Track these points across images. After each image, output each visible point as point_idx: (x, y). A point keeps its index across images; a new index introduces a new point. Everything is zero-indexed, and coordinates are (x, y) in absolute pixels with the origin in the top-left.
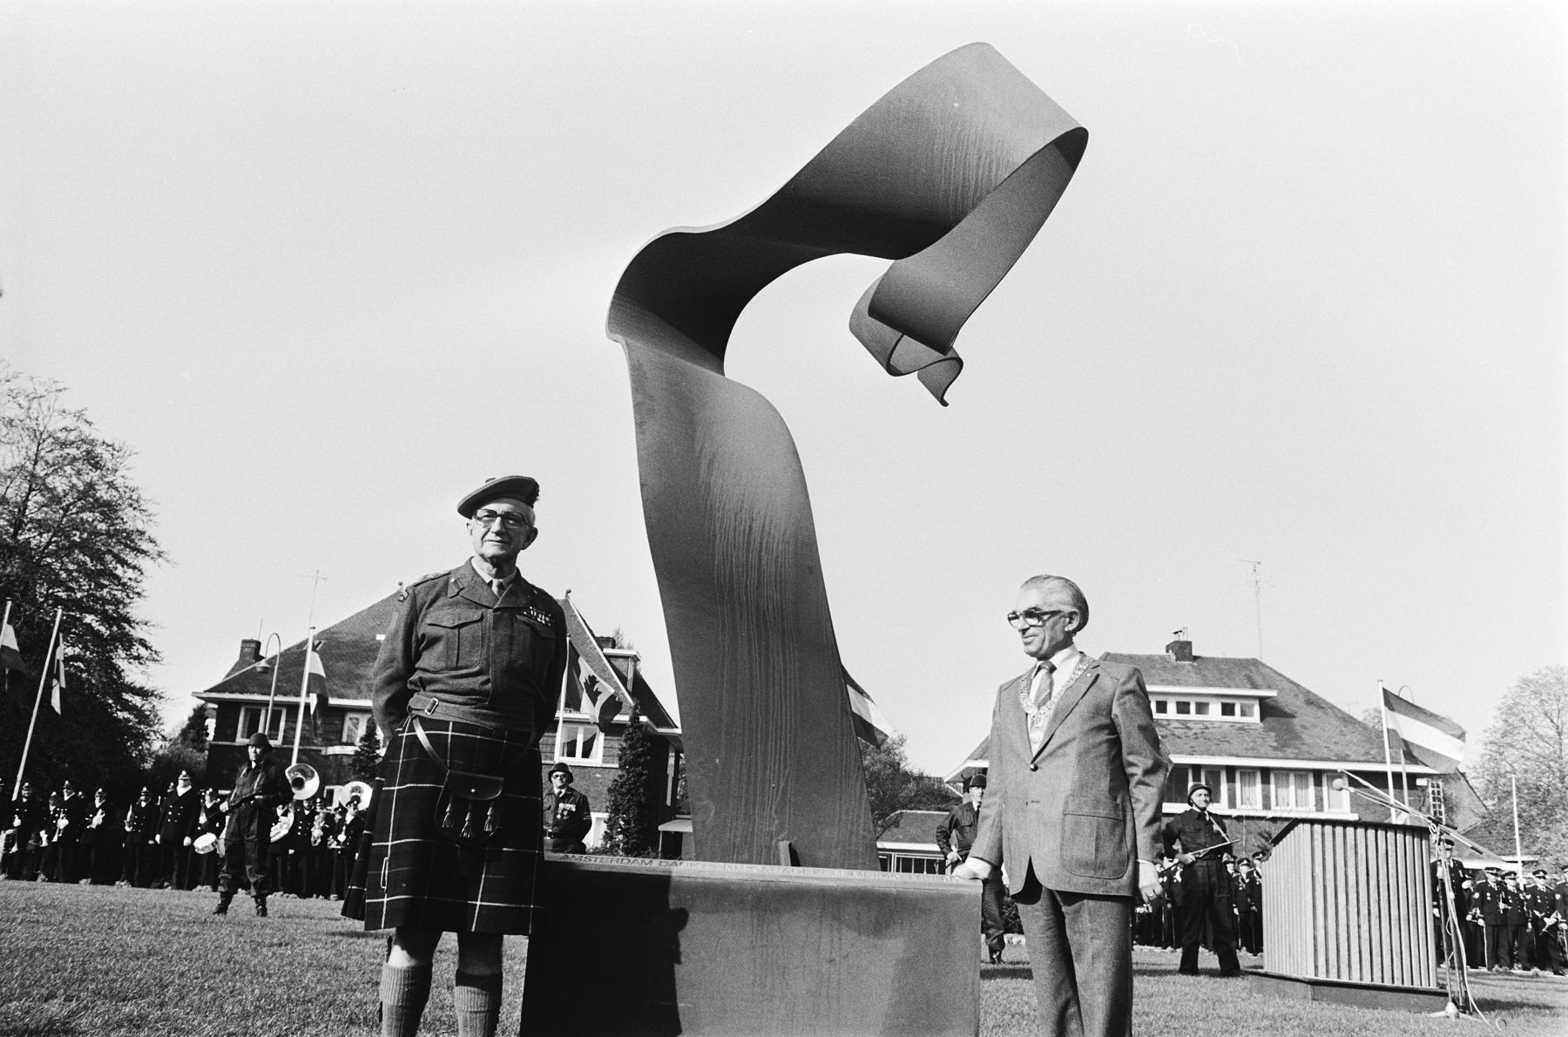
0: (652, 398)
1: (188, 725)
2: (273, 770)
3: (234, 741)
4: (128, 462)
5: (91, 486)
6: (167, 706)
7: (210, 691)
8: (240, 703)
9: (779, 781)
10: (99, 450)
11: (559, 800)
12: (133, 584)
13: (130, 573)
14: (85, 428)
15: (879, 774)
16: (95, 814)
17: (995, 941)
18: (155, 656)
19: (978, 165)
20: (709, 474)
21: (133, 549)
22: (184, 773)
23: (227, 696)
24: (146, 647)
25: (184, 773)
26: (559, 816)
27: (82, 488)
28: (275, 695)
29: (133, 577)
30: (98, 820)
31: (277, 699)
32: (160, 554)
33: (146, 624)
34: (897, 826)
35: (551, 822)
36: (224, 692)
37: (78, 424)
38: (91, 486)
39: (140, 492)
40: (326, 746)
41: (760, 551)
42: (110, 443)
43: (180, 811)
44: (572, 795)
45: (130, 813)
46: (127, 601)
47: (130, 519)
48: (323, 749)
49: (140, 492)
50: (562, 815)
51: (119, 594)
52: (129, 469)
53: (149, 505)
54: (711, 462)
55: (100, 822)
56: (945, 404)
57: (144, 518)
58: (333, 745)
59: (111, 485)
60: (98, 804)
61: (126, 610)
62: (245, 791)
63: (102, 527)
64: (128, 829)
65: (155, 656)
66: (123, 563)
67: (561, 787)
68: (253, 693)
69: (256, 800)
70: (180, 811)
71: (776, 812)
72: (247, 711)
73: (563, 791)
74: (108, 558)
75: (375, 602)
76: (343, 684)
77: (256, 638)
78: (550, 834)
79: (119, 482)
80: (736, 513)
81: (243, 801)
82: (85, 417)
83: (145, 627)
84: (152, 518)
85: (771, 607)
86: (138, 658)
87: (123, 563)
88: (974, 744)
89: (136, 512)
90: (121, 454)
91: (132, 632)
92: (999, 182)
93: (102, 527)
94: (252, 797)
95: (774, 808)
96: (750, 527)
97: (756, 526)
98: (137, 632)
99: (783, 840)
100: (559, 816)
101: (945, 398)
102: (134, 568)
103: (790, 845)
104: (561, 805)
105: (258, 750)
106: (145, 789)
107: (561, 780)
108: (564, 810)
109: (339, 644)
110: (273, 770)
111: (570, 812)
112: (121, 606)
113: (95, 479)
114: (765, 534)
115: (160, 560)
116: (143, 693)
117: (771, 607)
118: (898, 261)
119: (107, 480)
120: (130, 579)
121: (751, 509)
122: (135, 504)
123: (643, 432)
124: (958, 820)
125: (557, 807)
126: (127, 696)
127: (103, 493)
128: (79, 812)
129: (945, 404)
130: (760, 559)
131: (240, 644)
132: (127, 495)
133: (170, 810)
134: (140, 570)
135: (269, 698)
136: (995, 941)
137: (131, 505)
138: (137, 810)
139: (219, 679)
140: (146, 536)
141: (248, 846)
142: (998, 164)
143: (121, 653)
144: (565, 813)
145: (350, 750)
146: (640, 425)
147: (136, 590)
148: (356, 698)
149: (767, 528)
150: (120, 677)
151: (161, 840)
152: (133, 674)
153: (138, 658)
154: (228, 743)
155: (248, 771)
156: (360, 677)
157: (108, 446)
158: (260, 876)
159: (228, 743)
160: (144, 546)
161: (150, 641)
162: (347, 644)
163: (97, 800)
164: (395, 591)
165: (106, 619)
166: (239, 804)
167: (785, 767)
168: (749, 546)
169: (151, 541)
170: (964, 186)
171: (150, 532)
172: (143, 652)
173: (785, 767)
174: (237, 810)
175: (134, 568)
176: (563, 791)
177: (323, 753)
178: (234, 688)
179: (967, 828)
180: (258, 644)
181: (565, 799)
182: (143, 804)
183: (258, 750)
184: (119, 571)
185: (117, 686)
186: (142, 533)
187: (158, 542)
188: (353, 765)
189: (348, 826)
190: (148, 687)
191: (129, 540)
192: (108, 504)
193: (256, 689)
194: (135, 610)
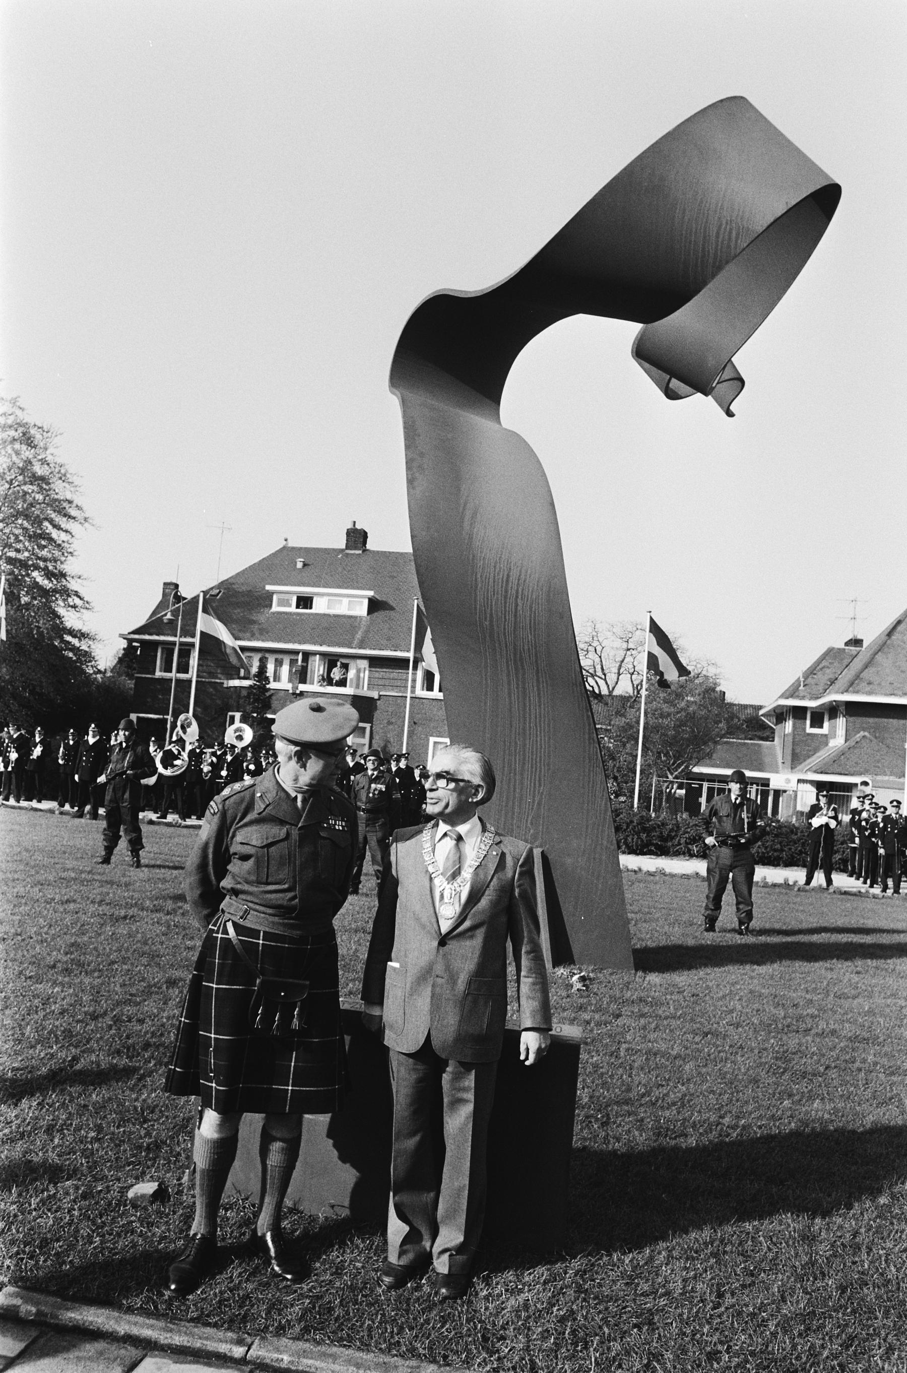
0: (422, 455)
1: (123, 655)
2: (139, 749)
3: (154, 674)
4: (56, 441)
5: (29, 462)
6: (100, 646)
7: (134, 632)
8: (156, 644)
9: (534, 797)
10: (33, 431)
11: (372, 780)
12: (66, 545)
13: (63, 536)
14: (19, 412)
15: (694, 713)
16: (35, 747)
17: (743, 915)
18: (87, 606)
19: (717, 236)
20: (471, 525)
21: (65, 515)
22: (93, 726)
23: (147, 637)
24: (81, 598)
25: (93, 726)
26: (371, 795)
27: (21, 465)
28: (181, 636)
29: (65, 539)
30: (37, 751)
31: (183, 640)
32: (86, 519)
33: (79, 578)
34: (710, 758)
35: (364, 799)
36: (144, 634)
37: (13, 410)
38: (29, 462)
39: (67, 467)
40: (228, 679)
41: (517, 597)
42: (40, 425)
43: (92, 757)
44: (383, 777)
45: (62, 749)
46: (63, 559)
47: (61, 490)
48: (225, 682)
49: (67, 467)
50: (374, 794)
51: (57, 553)
52: (57, 447)
53: (75, 477)
54: (475, 514)
55: (39, 754)
56: (730, 414)
57: (72, 489)
58: (233, 679)
59: (44, 462)
60: (38, 740)
61: (62, 566)
62: (119, 766)
63: (40, 497)
64: (61, 762)
65: (87, 606)
66: (57, 527)
67: (373, 770)
68: (168, 635)
69: (127, 775)
70: (92, 757)
71: (532, 824)
72: (163, 649)
73: (376, 773)
74: (46, 524)
75: (264, 556)
76: (240, 628)
77: (174, 581)
78: (363, 810)
79: (49, 458)
80: (496, 563)
81: (117, 775)
82: (18, 404)
83: (79, 580)
84: (78, 489)
85: (526, 647)
86: (74, 607)
87: (57, 527)
88: (786, 683)
89: (64, 484)
90: (49, 434)
91: (69, 586)
92: (738, 251)
93: (40, 497)
94: (124, 773)
95: (530, 818)
96: (508, 576)
97: (514, 574)
98: (73, 585)
99: (537, 847)
100: (371, 795)
101: (731, 408)
102: (66, 531)
103: (542, 853)
104: (373, 786)
105: (127, 733)
106: (72, 731)
107: (373, 763)
108: (375, 789)
109: (236, 593)
110: (139, 749)
111: (380, 791)
112: (59, 562)
113: (31, 456)
114: (521, 581)
115: (86, 525)
116: (81, 635)
117: (526, 647)
118: (650, 325)
119: (40, 457)
120: (63, 541)
121: (509, 563)
122: (63, 478)
123: (414, 488)
124: (716, 810)
125: (370, 787)
126: (68, 638)
127: (39, 470)
128: (24, 746)
129: (730, 414)
130: (517, 605)
131: (162, 586)
132: (57, 470)
133: (84, 756)
134: (71, 534)
135: (176, 639)
136: (743, 915)
137: (60, 478)
138: (67, 746)
139: (141, 621)
140: (74, 505)
141: (123, 810)
142: (738, 234)
143: (61, 603)
144: (376, 792)
145: (246, 683)
146: (411, 482)
147: (69, 550)
148: (249, 640)
149: (523, 577)
150: (62, 623)
151: (79, 778)
152: (71, 619)
153: (74, 607)
154: (150, 676)
155: (120, 750)
156: (254, 622)
157: (39, 428)
158: (134, 835)
159: (150, 676)
160: (73, 512)
161: (82, 593)
162: (243, 594)
163: (37, 736)
164: (281, 546)
165: (49, 575)
166: (114, 778)
167: (540, 785)
168: (506, 592)
169: (78, 507)
170: (703, 256)
171: (77, 501)
172: (77, 601)
173: (540, 785)
174: (113, 782)
175: (66, 531)
176: (376, 773)
177: (225, 686)
178: (152, 631)
179: (725, 818)
180: (177, 586)
181: (376, 780)
182: (71, 742)
183: (127, 733)
184: (55, 534)
185: (60, 630)
186: (70, 502)
187: (84, 509)
188: (248, 697)
189: (229, 764)
190: (85, 630)
191: (61, 507)
192: (43, 479)
193: (169, 632)
194: (69, 566)
